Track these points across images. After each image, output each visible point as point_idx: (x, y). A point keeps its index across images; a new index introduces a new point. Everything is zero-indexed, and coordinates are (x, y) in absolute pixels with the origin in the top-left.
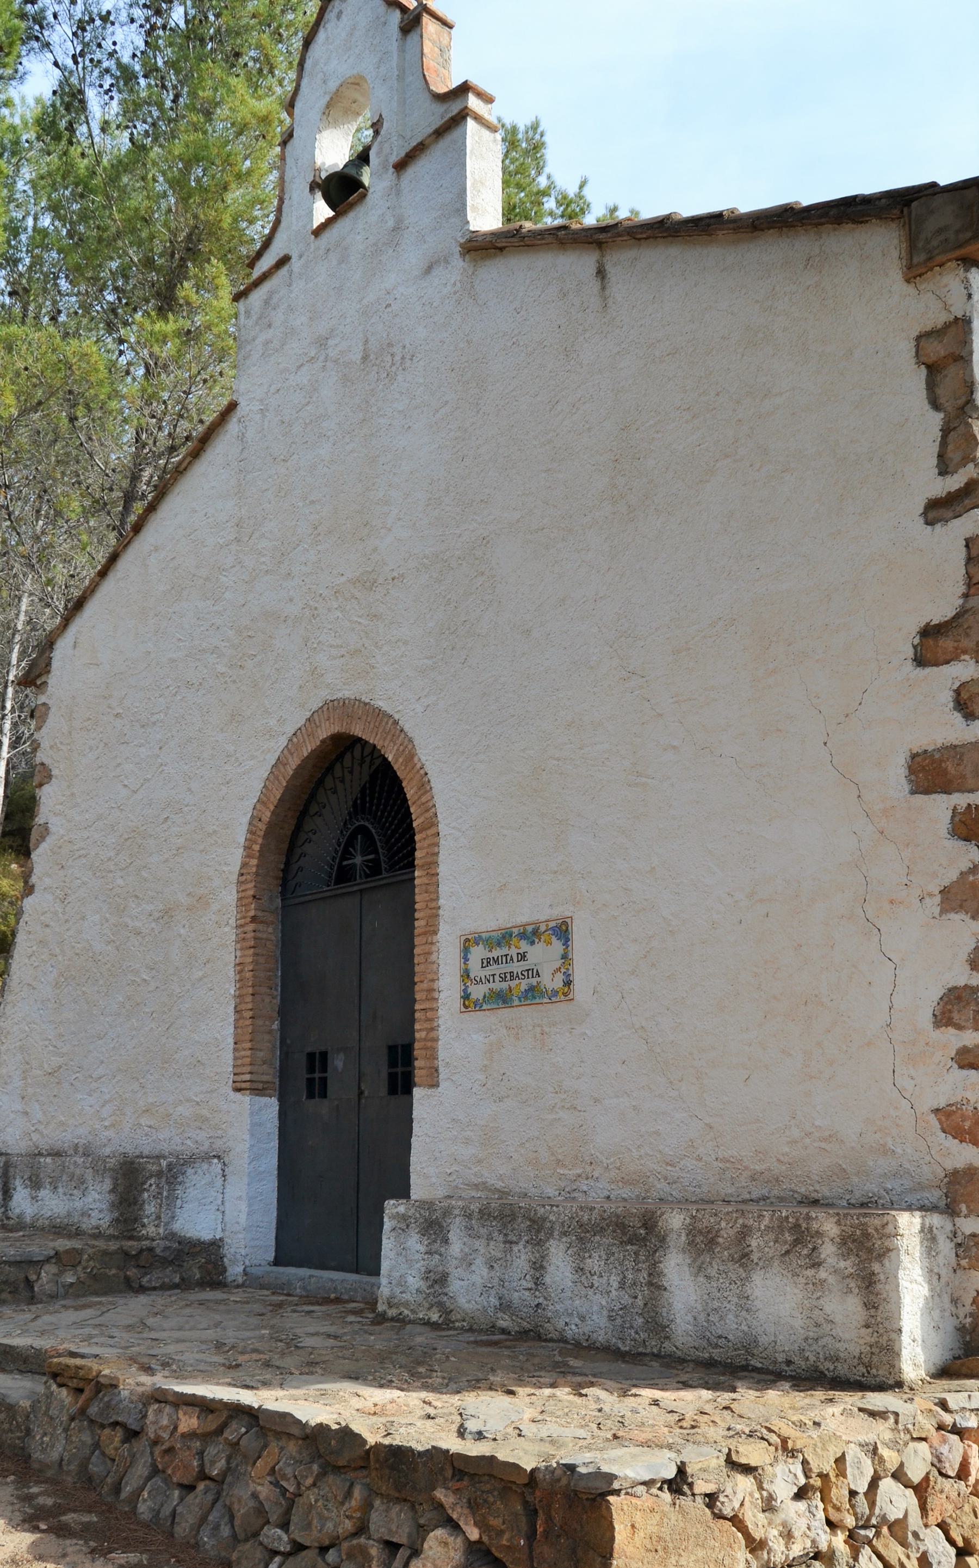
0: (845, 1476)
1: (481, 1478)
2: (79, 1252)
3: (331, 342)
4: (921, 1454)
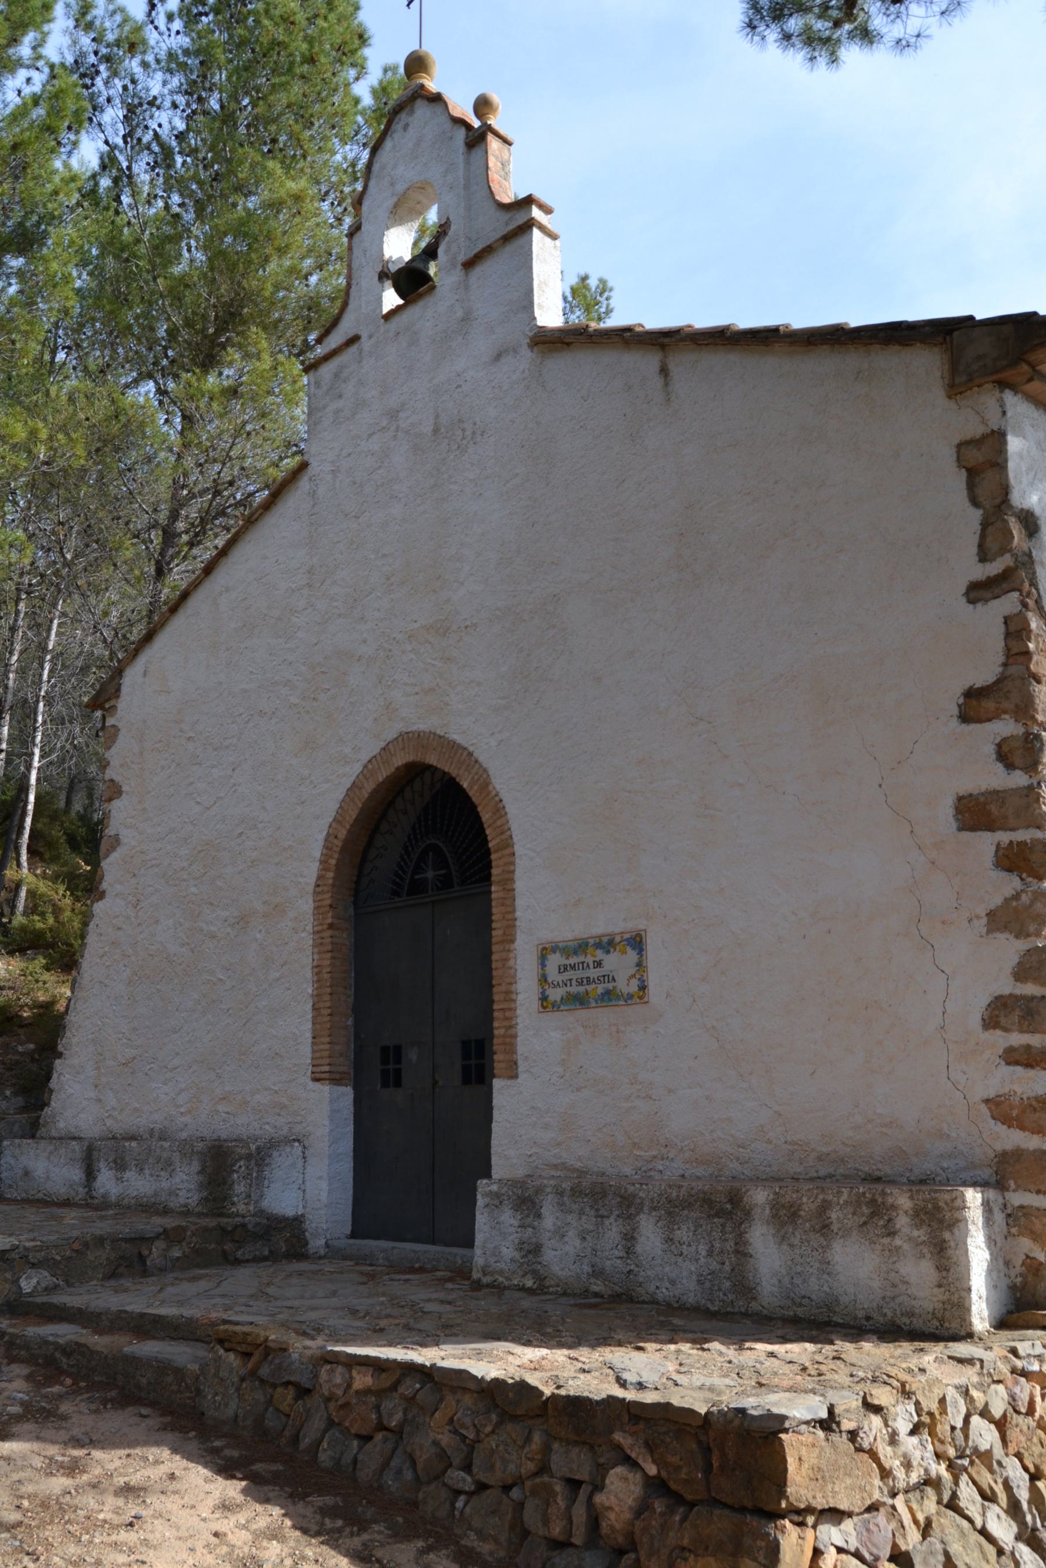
0: (947, 1414)
1: (660, 1423)
2: (184, 1229)
3: (402, 415)
4: (1000, 1394)
